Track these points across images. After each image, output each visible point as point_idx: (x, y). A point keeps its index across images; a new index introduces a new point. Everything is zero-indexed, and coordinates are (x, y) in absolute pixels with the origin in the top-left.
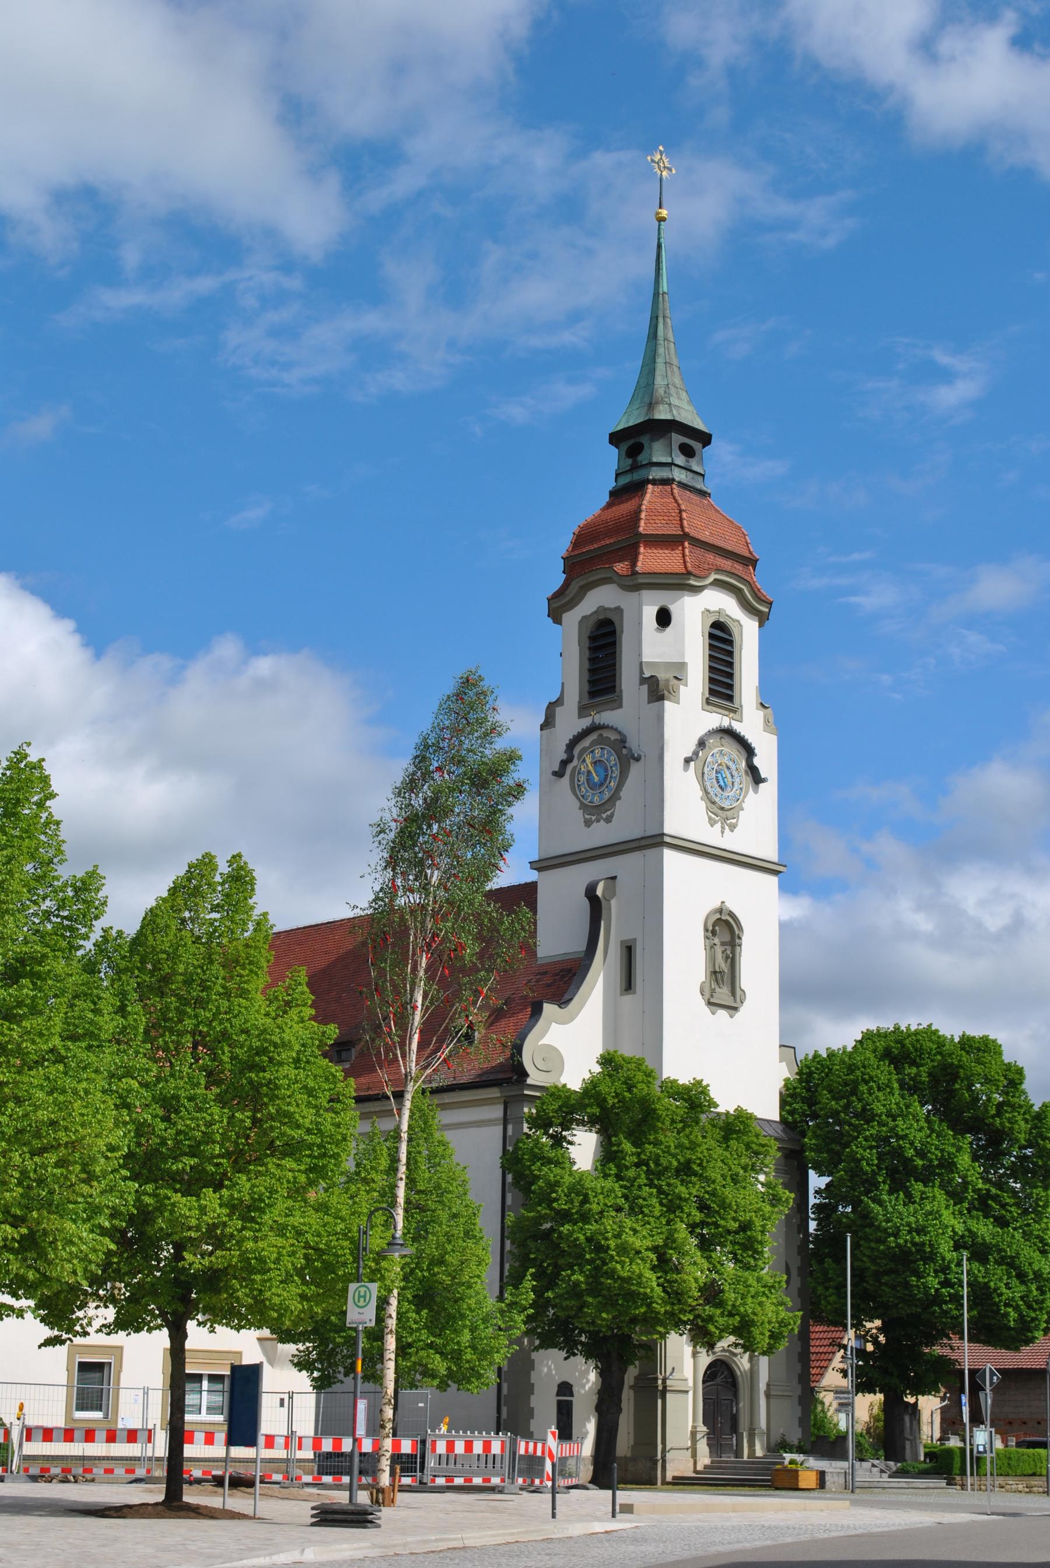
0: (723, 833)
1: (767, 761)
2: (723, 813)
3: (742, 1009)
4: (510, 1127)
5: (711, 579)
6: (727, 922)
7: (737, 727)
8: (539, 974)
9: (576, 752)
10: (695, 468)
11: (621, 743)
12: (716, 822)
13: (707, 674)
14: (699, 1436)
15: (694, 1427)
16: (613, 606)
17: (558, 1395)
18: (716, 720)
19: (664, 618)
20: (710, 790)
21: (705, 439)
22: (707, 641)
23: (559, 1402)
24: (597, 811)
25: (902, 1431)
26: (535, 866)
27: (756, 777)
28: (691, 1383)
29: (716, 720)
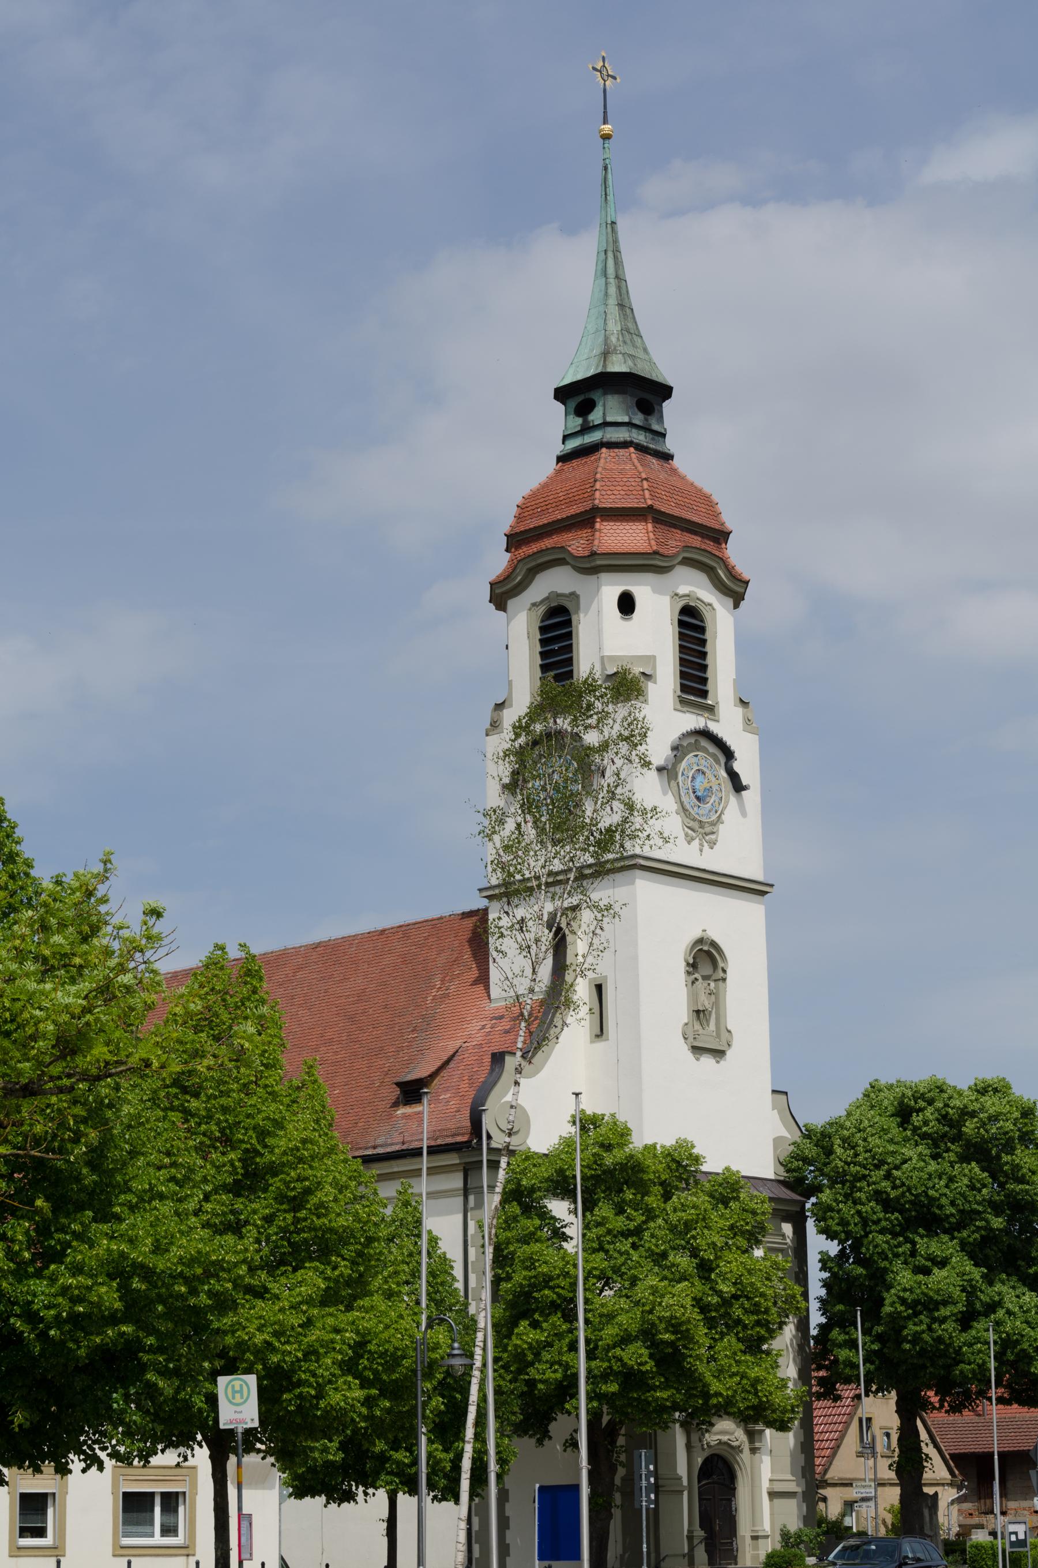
0: (701, 851)
2: (703, 829)
4: (471, 1198)
5: (680, 558)
6: (708, 953)
7: (714, 727)
8: (496, 1018)
10: (656, 427)
12: (693, 839)
14: (696, 1542)
16: (567, 591)
18: (692, 721)
19: (626, 604)
20: (688, 807)
22: (677, 629)
27: (738, 786)
28: (685, 1483)
29: (692, 721)
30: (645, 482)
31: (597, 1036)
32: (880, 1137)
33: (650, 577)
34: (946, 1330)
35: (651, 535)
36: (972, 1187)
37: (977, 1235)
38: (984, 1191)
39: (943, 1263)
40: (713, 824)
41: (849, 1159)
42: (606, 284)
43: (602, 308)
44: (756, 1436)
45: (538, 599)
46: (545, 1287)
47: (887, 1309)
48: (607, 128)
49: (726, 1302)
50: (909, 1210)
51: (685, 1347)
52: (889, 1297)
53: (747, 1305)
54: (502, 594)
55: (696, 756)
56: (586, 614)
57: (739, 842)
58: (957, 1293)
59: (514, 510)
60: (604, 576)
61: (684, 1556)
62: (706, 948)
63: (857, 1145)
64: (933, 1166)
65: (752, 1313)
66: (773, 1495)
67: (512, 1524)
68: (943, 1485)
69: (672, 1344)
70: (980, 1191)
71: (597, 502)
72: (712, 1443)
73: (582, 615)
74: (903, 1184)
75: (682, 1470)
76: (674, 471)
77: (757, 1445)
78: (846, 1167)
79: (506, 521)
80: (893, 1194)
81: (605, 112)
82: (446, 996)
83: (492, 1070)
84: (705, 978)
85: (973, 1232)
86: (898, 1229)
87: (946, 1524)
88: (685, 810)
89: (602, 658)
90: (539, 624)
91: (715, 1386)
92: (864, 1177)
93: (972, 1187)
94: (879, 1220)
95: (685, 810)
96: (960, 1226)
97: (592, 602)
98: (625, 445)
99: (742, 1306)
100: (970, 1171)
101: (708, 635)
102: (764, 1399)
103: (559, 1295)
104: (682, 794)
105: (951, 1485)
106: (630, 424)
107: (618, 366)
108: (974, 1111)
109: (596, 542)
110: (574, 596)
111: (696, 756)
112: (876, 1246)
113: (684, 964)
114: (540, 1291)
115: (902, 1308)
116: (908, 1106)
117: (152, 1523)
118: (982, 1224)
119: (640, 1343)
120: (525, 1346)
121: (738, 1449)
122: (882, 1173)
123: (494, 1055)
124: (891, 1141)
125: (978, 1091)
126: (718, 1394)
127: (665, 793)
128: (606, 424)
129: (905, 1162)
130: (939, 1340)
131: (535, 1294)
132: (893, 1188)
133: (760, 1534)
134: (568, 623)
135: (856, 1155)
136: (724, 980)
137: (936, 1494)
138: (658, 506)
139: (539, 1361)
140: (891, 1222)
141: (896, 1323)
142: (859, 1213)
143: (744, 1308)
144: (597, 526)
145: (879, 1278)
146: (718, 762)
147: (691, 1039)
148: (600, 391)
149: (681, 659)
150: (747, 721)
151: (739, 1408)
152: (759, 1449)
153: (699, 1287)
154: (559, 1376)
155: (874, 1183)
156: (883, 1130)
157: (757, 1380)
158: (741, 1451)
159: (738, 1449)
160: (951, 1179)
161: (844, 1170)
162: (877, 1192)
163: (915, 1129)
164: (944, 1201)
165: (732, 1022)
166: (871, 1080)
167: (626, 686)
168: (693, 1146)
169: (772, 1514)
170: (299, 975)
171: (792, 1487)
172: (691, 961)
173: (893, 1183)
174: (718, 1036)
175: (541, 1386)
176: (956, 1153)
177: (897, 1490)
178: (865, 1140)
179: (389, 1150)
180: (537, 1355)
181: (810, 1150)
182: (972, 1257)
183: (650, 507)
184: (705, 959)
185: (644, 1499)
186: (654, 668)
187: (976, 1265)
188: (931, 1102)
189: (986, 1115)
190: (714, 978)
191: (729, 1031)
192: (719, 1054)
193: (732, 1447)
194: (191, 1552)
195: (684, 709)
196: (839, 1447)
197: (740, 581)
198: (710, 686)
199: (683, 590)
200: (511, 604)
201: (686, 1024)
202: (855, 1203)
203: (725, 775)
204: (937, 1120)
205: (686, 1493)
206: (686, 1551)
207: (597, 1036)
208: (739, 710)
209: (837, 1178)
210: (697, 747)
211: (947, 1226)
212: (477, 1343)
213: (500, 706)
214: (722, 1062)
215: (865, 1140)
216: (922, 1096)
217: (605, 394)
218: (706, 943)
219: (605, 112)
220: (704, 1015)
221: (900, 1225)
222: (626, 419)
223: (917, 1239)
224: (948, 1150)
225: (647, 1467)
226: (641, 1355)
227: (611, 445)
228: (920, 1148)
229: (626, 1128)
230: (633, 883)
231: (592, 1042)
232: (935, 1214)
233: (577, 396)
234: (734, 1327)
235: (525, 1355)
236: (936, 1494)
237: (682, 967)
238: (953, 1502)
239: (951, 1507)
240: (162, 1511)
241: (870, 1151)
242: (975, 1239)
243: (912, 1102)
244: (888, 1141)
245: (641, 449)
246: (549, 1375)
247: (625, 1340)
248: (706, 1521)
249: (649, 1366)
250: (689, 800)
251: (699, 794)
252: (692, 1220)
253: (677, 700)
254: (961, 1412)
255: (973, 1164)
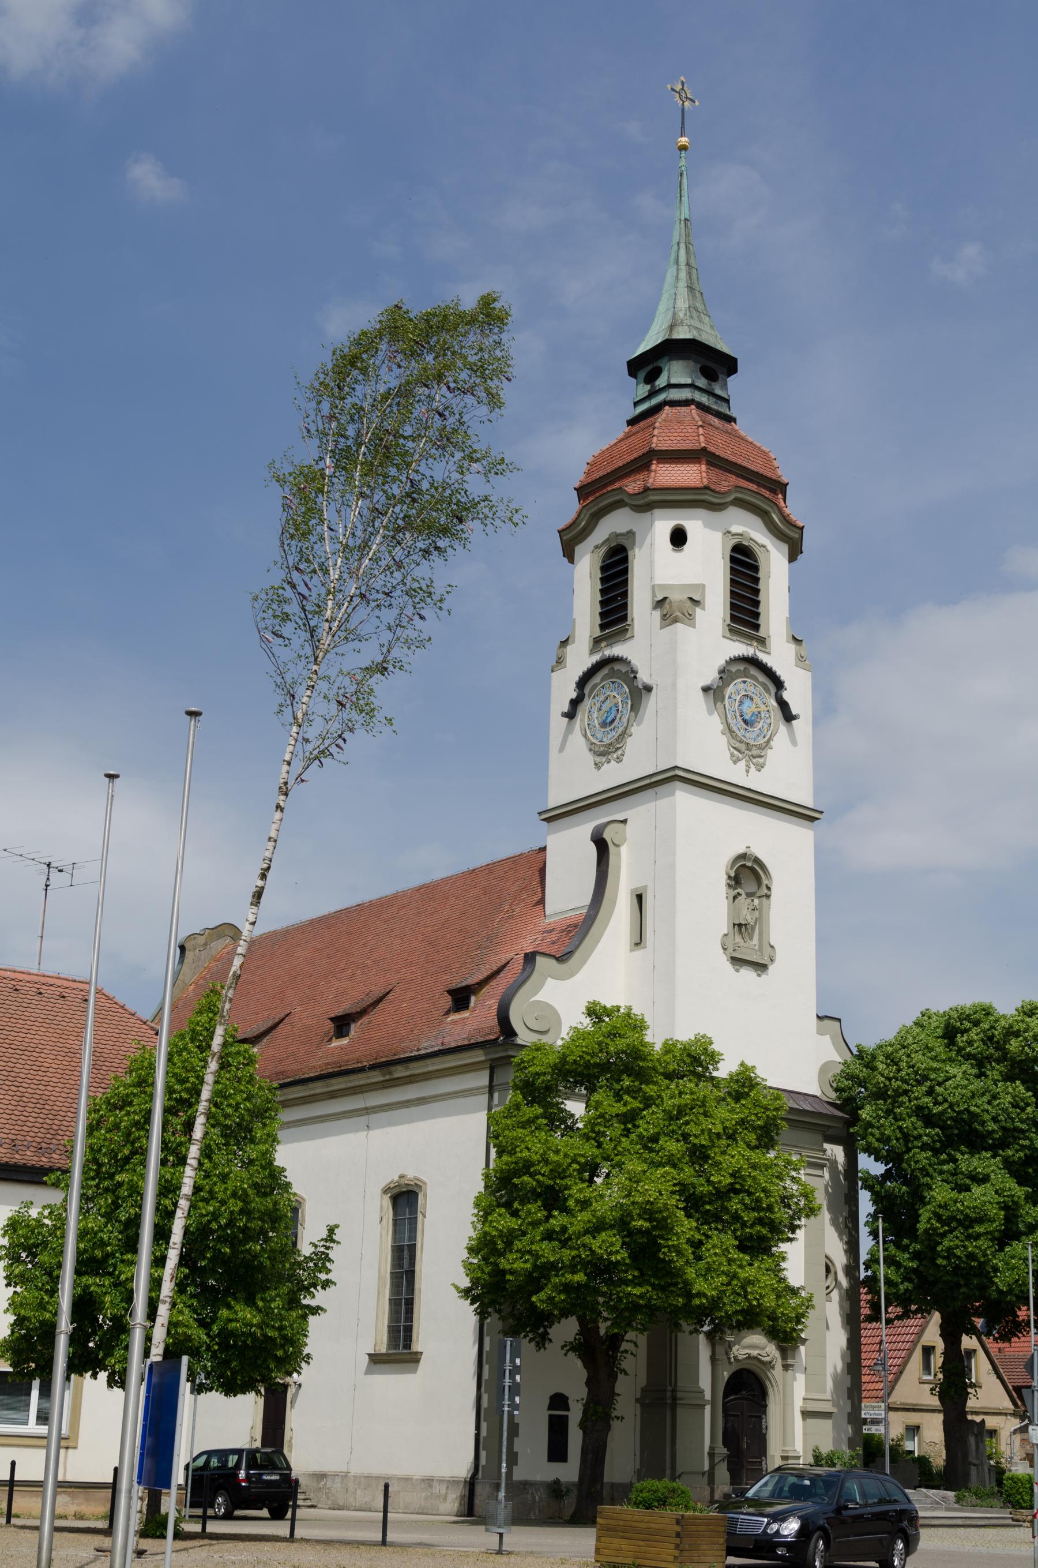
0: (748, 772)
1: (798, 691)
2: (751, 752)
3: (771, 968)
4: (496, 1095)
5: (732, 497)
6: (752, 869)
7: (762, 657)
8: (547, 932)
9: (587, 691)
10: (718, 392)
11: (630, 675)
12: (739, 760)
13: (728, 600)
14: (717, 1460)
15: (711, 1448)
16: (624, 531)
17: (549, 1408)
18: (741, 649)
19: (679, 538)
20: (735, 729)
21: (729, 365)
22: (728, 564)
23: (550, 1416)
24: (605, 752)
25: (966, 1455)
26: (544, 816)
27: (789, 717)
28: (708, 1396)
29: (741, 649)
30: (701, 429)
31: (637, 944)
32: (924, 1055)
33: (702, 512)
34: (979, 1248)
35: (704, 475)
36: (1015, 1106)
37: (1022, 1154)
38: (1029, 1109)
39: (984, 1179)
40: (760, 748)
41: (891, 1075)
42: (678, 270)
43: (672, 292)
44: (789, 1353)
45: (600, 542)
46: (525, 1174)
47: (922, 1226)
48: (684, 140)
49: (722, 1194)
50: (950, 1127)
51: (662, 1237)
52: (925, 1214)
53: (747, 1200)
54: (570, 542)
55: (744, 682)
56: (641, 547)
57: (788, 767)
58: (993, 1211)
59: (585, 468)
60: (657, 512)
61: (703, 1474)
62: (749, 864)
63: (900, 1060)
64: (977, 1085)
65: (753, 1209)
66: (806, 1414)
67: (521, 1430)
68: (1006, 1414)
69: (647, 1232)
70: (1023, 1110)
71: (653, 445)
72: (740, 1357)
73: (637, 550)
74: (946, 1100)
75: (705, 1381)
76: (735, 435)
77: (790, 1361)
78: (887, 1083)
79: (578, 476)
80: (936, 1110)
81: (683, 123)
82: (511, 917)
83: (524, 969)
84: (749, 895)
85: (1017, 1151)
86: (938, 1145)
87: (1009, 1453)
88: (731, 731)
89: (653, 586)
90: (600, 564)
91: (700, 1286)
92: (906, 1092)
93: (1015, 1106)
94: (920, 1136)
95: (731, 731)
96: (1003, 1144)
97: (647, 535)
98: (686, 403)
99: (742, 1202)
100: (1014, 1090)
101: (761, 574)
102: (755, 1303)
103: (538, 1181)
104: (729, 716)
105: (1014, 1414)
106: (692, 386)
107: (682, 334)
108: (1019, 1031)
109: (651, 480)
110: (631, 534)
111: (744, 682)
112: (917, 1162)
113: (725, 877)
114: (520, 1177)
115: (938, 1225)
116: (954, 1027)
117: (27, 1408)
118: (1027, 1143)
119: (615, 1231)
120: (494, 1233)
121: (770, 1365)
122: (924, 1088)
123: (526, 955)
124: (934, 1059)
125: (1025, 1013)
126: (701, 1294)
127: (710, 713)
128: (670, 386)
129: (948, 1079)
130: (971, 1256)
131: (515, 1181)
132: (935, 1105)
133: (790, 1454)
134: (625, 560)
135: (899, 1070)
136: (768, 896)
137: (983, 1421)
138: (711, 449)
139: (511, 1251)
140: (932, 1137)
141: (932, 1238)
142: (900, 1128)
143: (744, 1204)
144: (653, 467)
145: (917, 1196)
146: (768, 691)
147: (730, 950)
148: (666, 358)
149: (732, 592)
150: (800, 659)
151: (726, 1312)
152: (792, 1366)
153: (687, 1174)
154: (528, 1266)
155: (917, 1099)
156: (927, 1047)
157: (749, 1282)
158: (773, 1368)
159: (770, 1365)
160: (995, 1097)
161: (885, 1085)
162: (919, 1108)
163: (960, 1050)
164: (986, 1117)
165: (775, 937)
166: (923, 1009)
167: (672, 610)
168: (711, 1043)
169: (804, 1434)
170: (401, 912)
171: (827, 1407)
172: (733, 875)
173: (935, 1099)
174: (761, 950)
175: (509, 1277)
176: (1001, 1072)
177: (940, 1417)
178: (909, 1056)
179: (429, 1051)
180: (509, 1244)
181: (858, 1069)
182: (1014, 1174)
183: (704, 449)
184: (747, 874)
185: (507, 1402)
186: (703, 595)
187: (1020, 1184)
188: (976, 1023)
189: (1031, 1034)
190: (758, 894)
191: (772, 947)
192: (761, 967)
193: (763, 1362)
194: (71, 1444)
195: (734, 638)
196: (901, 1372)
197: (795, 526)
198: (762, 621)
199: (736, 529)
200: (578, 550)
201: (726, 935)
202: (896, 1120)
203: (775, 704)
204: (982, 1040)
205: (708, 1409)
206: (706, 1468)
207: (637, 944)
208: (792, 647)
209: (880, 1094)
210: (746, 674)
211: (991, 1142)
212: (189, 1161)
213: (564, 643)
214: (763, 976)
215: (909, 1056)
216: (968, 1017)
217: (670, 360)
218: (750, 859)
219: (683, 123)
220: (746, 929)
221: (940, 1141)
222: (689, 381)
223: (959, 1156)
224: (993, 1068)
225: (513, 1361)
226: (612, 1244)
227: (673, 404)
228: (964, 1067)
229: (642, 1021)
230: (673, 794)
231: (631, 951)
232: (976, 1130)
233: (645, 366)
234: (731, 1224)
235: (496, 1244)
236: (983, 1421)
237: (723, 880)
238: (1015, 1432)
239: (1014, 1437)
240: (40, 1394)
241: (913, 1067)
242: (1020, 1158)
243: (958, 1024)
244: (931, 1059)
245: (700, 406)
246: (519, 1265)
247: (597, 1228)
248: (730, 1438)
249: (622, 1255)
250: (737, 724)
251: (747, 717)
252: (686, 1105)
253: (727, 628)
254: (1009, 1341)
255: (1018, 1082)
